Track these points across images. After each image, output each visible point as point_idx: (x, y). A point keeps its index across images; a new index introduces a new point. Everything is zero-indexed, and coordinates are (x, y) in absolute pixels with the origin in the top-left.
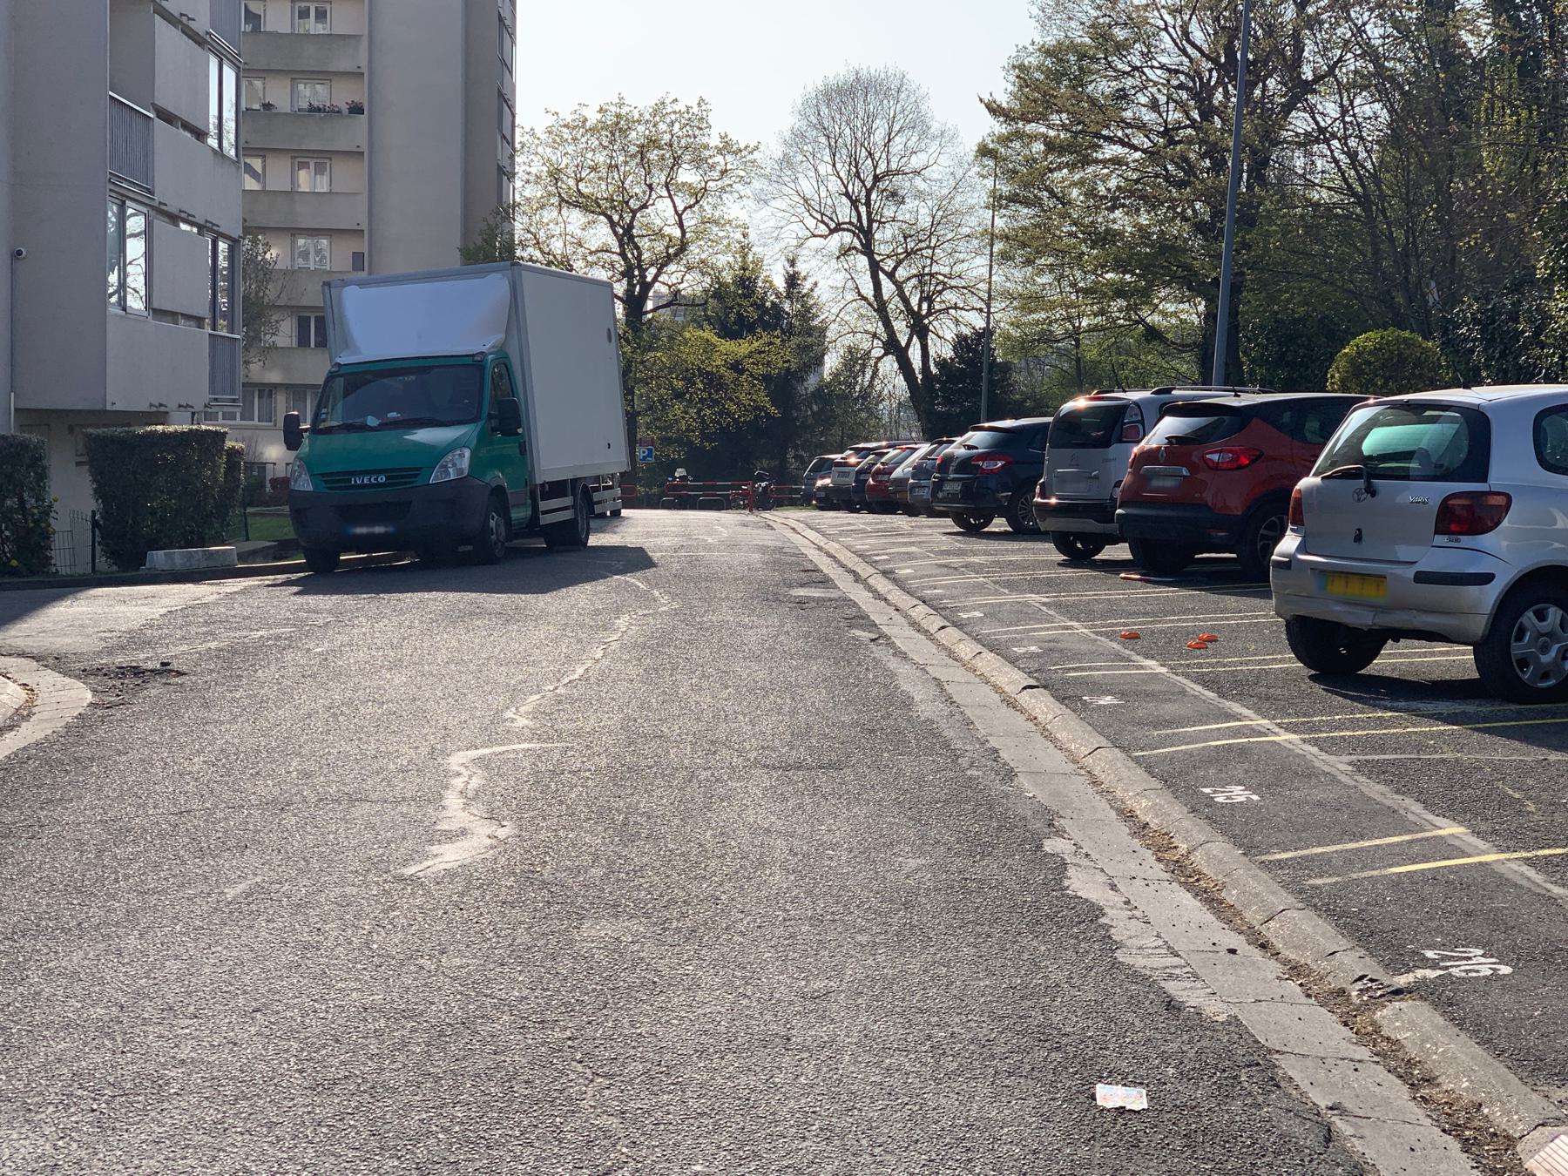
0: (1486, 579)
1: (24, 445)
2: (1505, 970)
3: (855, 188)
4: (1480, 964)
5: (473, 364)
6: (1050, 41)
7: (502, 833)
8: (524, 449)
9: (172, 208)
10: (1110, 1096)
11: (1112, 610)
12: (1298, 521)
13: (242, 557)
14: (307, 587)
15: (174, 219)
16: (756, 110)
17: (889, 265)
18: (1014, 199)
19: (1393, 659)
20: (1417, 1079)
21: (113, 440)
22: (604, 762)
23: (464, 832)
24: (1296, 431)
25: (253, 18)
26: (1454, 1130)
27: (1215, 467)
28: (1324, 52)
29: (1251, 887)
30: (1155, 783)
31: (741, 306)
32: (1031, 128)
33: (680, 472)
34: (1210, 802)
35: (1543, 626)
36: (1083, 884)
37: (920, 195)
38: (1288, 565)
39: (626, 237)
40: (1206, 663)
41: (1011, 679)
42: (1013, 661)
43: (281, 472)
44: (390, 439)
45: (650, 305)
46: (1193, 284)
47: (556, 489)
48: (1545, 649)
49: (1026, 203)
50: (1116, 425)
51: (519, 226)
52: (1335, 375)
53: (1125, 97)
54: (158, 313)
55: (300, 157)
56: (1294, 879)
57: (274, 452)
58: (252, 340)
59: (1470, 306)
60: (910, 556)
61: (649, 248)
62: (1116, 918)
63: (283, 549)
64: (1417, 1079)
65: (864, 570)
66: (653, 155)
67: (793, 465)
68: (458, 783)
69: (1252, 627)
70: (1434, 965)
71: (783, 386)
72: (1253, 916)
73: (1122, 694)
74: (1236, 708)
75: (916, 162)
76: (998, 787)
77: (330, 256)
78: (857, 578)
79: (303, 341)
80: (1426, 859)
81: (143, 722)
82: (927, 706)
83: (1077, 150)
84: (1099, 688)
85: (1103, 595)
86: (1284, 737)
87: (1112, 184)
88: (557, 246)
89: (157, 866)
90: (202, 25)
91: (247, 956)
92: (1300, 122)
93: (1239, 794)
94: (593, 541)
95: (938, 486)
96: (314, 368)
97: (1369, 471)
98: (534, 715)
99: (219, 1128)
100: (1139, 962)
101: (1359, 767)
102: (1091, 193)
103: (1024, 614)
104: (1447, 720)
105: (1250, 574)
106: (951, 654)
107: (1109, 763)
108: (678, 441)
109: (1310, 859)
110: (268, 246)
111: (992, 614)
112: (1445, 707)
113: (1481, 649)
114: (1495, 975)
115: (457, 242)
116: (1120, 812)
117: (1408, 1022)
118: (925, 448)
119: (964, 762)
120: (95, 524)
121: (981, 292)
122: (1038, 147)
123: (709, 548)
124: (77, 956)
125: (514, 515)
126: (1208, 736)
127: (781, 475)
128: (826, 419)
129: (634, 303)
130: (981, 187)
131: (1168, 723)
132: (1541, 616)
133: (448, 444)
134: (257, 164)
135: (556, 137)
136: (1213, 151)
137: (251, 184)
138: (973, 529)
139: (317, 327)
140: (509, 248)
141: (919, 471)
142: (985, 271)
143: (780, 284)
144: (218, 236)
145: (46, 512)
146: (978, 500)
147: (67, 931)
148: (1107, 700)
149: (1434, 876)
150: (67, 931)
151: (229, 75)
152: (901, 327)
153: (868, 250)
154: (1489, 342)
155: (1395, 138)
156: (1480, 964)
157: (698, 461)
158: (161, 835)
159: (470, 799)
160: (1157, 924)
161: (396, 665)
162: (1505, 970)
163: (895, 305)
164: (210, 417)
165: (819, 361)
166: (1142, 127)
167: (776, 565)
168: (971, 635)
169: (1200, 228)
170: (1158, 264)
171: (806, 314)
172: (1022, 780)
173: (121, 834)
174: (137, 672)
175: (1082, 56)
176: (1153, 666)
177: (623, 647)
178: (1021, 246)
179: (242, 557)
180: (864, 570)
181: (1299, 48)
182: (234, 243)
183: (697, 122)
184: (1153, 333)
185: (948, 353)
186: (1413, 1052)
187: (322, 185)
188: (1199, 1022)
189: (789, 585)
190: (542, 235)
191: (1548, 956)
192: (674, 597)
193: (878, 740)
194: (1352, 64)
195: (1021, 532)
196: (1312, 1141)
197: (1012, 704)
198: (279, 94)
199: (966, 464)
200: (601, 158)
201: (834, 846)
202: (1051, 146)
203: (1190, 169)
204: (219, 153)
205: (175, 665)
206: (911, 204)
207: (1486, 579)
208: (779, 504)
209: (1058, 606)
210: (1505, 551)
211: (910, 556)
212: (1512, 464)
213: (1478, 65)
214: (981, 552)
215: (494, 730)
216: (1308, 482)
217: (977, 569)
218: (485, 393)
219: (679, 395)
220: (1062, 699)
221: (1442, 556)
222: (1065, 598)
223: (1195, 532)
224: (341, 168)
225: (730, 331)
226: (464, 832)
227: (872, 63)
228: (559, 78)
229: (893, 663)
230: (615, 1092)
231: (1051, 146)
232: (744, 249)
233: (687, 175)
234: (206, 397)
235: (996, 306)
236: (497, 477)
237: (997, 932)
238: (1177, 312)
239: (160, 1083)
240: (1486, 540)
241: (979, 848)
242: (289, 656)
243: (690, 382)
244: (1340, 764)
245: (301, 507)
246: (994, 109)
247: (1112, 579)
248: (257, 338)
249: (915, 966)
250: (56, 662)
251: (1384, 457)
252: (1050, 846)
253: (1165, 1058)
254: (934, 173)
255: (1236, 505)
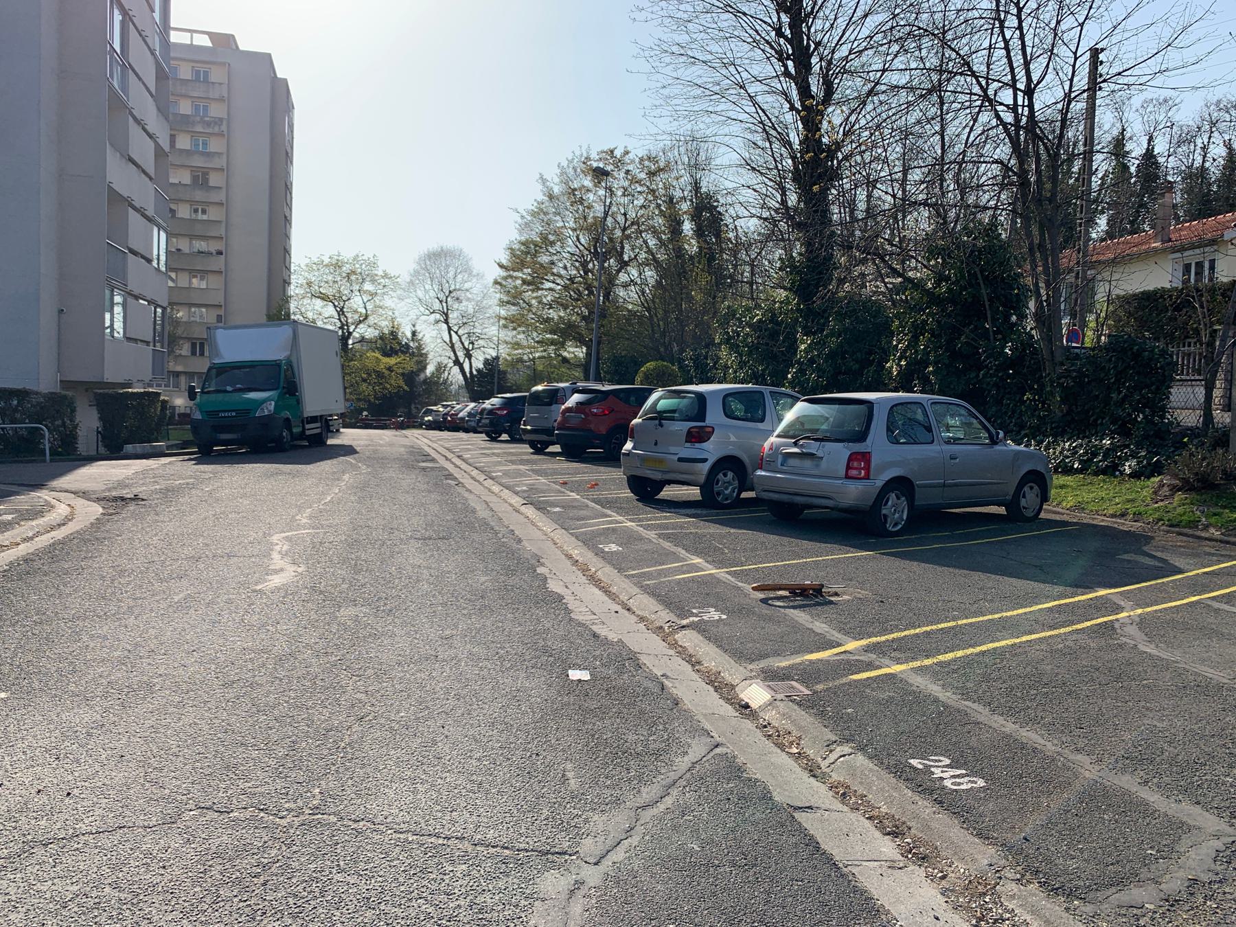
0: (705, 460)
1: (65, 397)
2: (724, 617)
3: (441, 296)
4: (713, 615)
5: (276, 365)
6: (523, 239)
7: (300, 570)
8: (299, 402)
9: (136, 292)
10: (575, 675)
11: (555, 472)
12: (632, 437)
13: (168, 447)
14: (199, 461)
15: (137, 298)
16: (399, 262)
17: (455, 328)
18: (508, 302)
19: (668, 492)
20: (694, 662)
21: (110, 396)
22: (344, 538)
23: (282, 570)
24: (627, 401)
25: (172, 211)
26: (711, 683)
27: (596, 414)
28: (633, 249)
29: (622, 586)
30: (580, 543)
31: (390, 344)
32: (515, 274)
33: (365, 413)
34: (603, 551)
35: (726, 479)
36: (554, 586)
37: (468, 299)
38: (628, 454)
39: (341, 312)
40: (595, 494)
41: (516, 501)
42: (517, 493)
43: (182, 411)
44: (236, 396)
45: (350, 342)
46: (581, 340)
47: (313, 419)
48: (726, 488)
49: (514, 304)
50: (554, 397)
51: (293, 306)
52: (638, 379)
53: (553, 263)
54: (129, 339)
55: (193, 273)
56: (638, 581)
57: (180, 402)
58: (171, 352)
59: (689, 353)
60: (469, 450)
61: (351, 317)
62: (569, 599)
63: (185, 444)
64: (694, 662)
65: (450, 455)
66: (353, 277)
67: (414, 411)
68: (278, 548)
69: (613, 479)
70: (697, 616)
71: (410, 377)
72: (623, 597)
73: (563, 507)
74: (609, 512)
75: (467, 286)
76: (515, 546)
77: (208, 316)
78: (447, 459)
79: (194, 353)
80: (689, 572)
81: (127, 521)
82: (483, 513)
83: (534, 283)
84: (554, 505)
85: (550, 466)
86: (629, 524)
87: (549, 298)
88: (310, 315)
89: (141, 586)
90: (150, 213)
91: (187, 626)
92: (623, 277)
93: (614, 547)
94: (329, 442)
95: (479, 421)
96: (202, 365)
97: (660, 417)
98: (310, 517)
99: (181, 705)
100: (580, 618)
101: (660, 536)
102: (540, 302)
103: (519, 474)
104: (690, 516)
105: (612, 457)
106: (490, 490)
107: (560, 535)
108: (364, 400)
109: (644, 573)
110: (178, 311)
111: (506, 474)
112: (693, 511)
113: (702, 488)
114: (720, 620)
115: (265, 311)
116: (566, 555)
117: (688, 639)
118: (472, 405)
119: (500, 535)
120: (98, 432)
121: (494, 341)
122: (519, 282)
123: (381, 445)
124: (106, 628)
125: (294, 430)
126: (598, 524)
127: (409, 415)
128: (428, 392)
129: (344, 339)
130: (496, 296)
131: (583, 519)
132: (725, 475)
133: (264, 400)
134: (173, 275)
135: (309, 268)
136: (589, 287)
137: (171, 284)
138: (493, 438)
139: (198, 347)
140: (288, 315)
141: (470, 414)
142: (496, 333)
143: (409, 335)
144: (157, 306)
145: (76, 427)
146: (496, 427)
147: (99, 617)
148: (557, 509)
149: (693, 579)
150: (99, 617)
151: (163, 235)
152: (461, 354)
153: (446, 322)
154: (697, 368)
155: (659, 284)
156: (713, 615)
157: (372, 408)
158: (141, 572)
159: (284, 555)
160: (587, 603)
161: (244, 496)
162: (724, 617)
163: (458, 345)
164: (151, 386)
165: (425, 368)
166: (560, 276)
167: (411, 453)
168: (500, 482)
169: (584, 318)
170: (567, 332)
171: (419, 348)
172: (525, 543)
173: (122, 573)
174: (123, 499)
175: (536, 246)
176: (574, 495)
177: (348, 488)
178: (514, 322)
179: (168, 447)
180: (450, 455)
181: (623, 248)
182: (164, 309)
183: (374, 265)
184: (565, 360)
185: (481, 366)
186: (691, 651)
187: (203, 285)
188: (606, 642)
189: (417, 460)
190: (303, 310)
191: (740, 611)
192: (368, 466)
193: (461, 526)
194: (644, 255)
195: (514, 440)
196: (657, 690)
197: (518, 511)
198: (184, 245)
199: (491, 412)
200: (330, 278)
201: (449, 572)
202: (524, 282)
203: (580, 294)
204: (158, 270)
205: (141, 496)
206: (464, 303)
207: (705, 460)
208: (408, 427)
209: (533, 470)
210: (712, 450)
211: (469, 450)
212: (714, 416)
213: (691, 257)
214: (497, 448)
215: (291, 524)
216: (636, 421)
217: (498, 455)
218: (282, 377)
219: (364, 380)
220: (538, 509)
221: (688, 451)
222: (535, 467)
223: (589, 439)
224: (211, 277)
225: (388, 353)
226: (282, 570)
227: (449, 243)
228: (309, 245)
229: (466, 495)
230: (362, 683)
231: (524, 282)
232: (393, 320)
233: (368, 286)
234: (151, 377)
235: (501, 347)
236: (287, 414)
237: (521, 607)
238: (575, 352)
239: (150, 687)
240: (705, 445)
241: (509, 572)
242: (194, 492)
243: (369, 375)
244: (652, 535)
245: (196, 427)
246: (501, 266)
247: (553, 459)
248: (173, 351)
249: (488, 623)
250: (84, 495)
251: (665, 412)
252: (539, 570)
253: (595, 658)
254: (475, 291)
255: (603, 430)
